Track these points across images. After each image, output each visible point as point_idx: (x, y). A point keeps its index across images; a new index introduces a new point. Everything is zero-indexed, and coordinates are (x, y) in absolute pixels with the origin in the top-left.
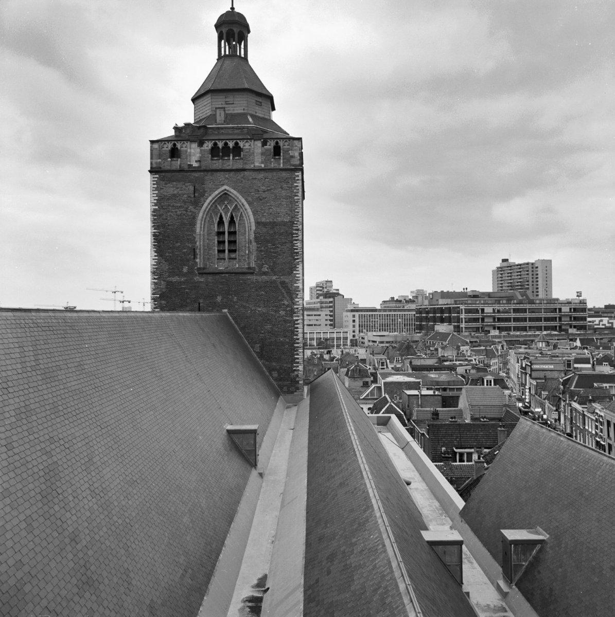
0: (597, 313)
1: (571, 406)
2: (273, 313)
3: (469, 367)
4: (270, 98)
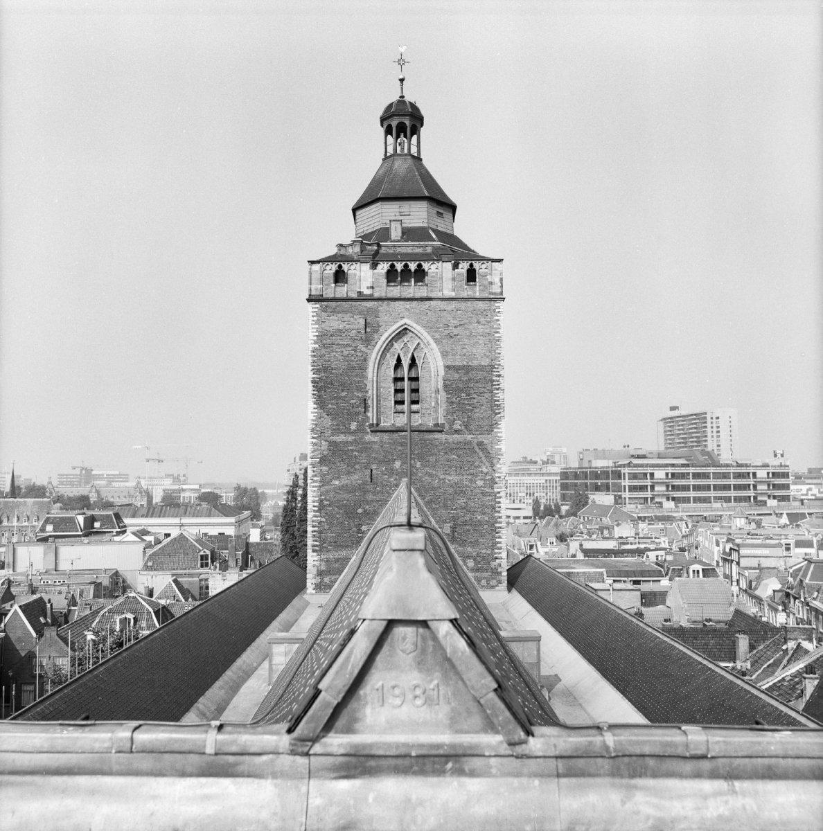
0: (799, 478)
2: (467, 483)
4: (453, 208)
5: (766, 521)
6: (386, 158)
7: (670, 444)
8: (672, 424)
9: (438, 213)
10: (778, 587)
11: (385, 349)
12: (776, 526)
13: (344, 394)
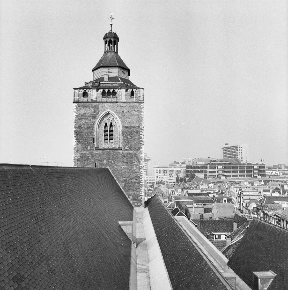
0: (270, 168)
1: (264, 212)
2: (130, 168)
3: (215, 194)
4: (128, 70)
5: (255, 183)
6: (105, 52)
7: (225, 157)
8: (226, 150)
9: (122, 72)
10: (255, 206)
11: (101, 120)
12: (259, 185)
13: (86, 136)
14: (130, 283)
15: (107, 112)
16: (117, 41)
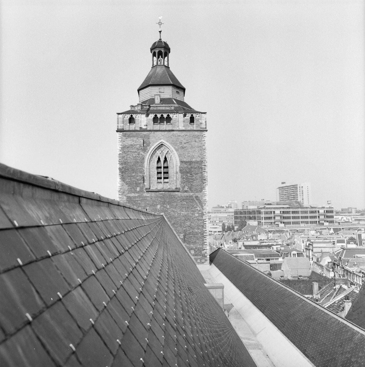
2: (191, 215)
3: (279, 246)
4: (184, 90)
5: (324, 232)
6: (153, 67)
7: (282, 199)
9: (177, 91)
10: (330, 260)
11: (152, 153)
14: (310, 362)
15: (160, 143)
16: (168, 52)
